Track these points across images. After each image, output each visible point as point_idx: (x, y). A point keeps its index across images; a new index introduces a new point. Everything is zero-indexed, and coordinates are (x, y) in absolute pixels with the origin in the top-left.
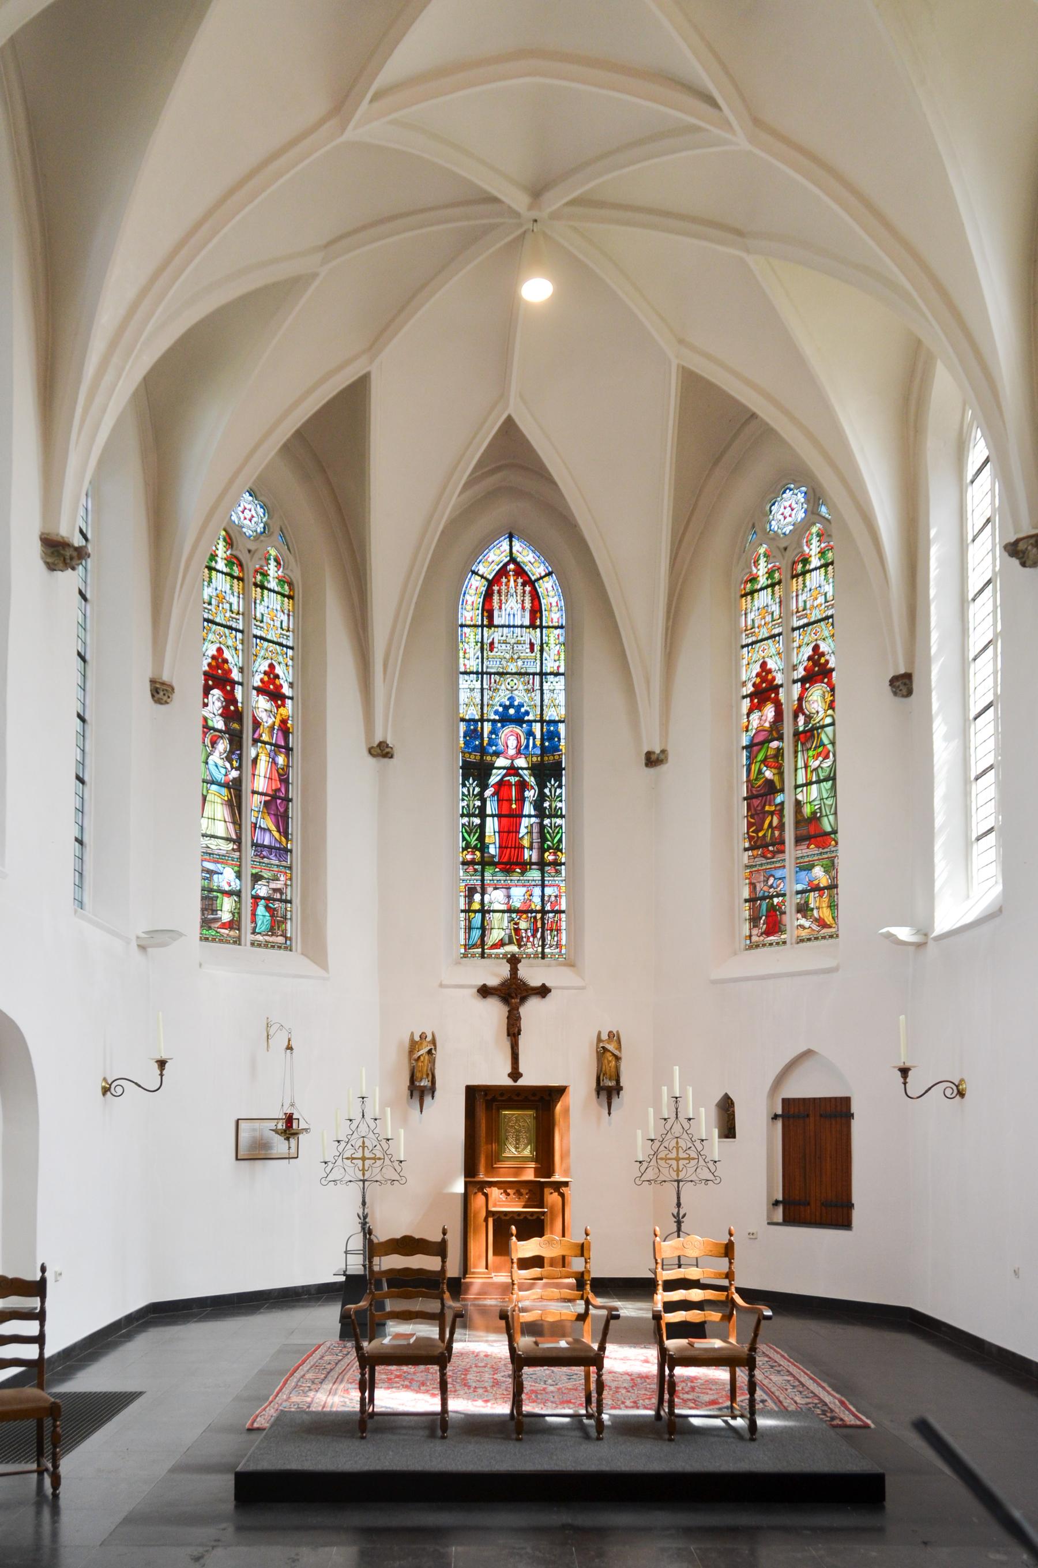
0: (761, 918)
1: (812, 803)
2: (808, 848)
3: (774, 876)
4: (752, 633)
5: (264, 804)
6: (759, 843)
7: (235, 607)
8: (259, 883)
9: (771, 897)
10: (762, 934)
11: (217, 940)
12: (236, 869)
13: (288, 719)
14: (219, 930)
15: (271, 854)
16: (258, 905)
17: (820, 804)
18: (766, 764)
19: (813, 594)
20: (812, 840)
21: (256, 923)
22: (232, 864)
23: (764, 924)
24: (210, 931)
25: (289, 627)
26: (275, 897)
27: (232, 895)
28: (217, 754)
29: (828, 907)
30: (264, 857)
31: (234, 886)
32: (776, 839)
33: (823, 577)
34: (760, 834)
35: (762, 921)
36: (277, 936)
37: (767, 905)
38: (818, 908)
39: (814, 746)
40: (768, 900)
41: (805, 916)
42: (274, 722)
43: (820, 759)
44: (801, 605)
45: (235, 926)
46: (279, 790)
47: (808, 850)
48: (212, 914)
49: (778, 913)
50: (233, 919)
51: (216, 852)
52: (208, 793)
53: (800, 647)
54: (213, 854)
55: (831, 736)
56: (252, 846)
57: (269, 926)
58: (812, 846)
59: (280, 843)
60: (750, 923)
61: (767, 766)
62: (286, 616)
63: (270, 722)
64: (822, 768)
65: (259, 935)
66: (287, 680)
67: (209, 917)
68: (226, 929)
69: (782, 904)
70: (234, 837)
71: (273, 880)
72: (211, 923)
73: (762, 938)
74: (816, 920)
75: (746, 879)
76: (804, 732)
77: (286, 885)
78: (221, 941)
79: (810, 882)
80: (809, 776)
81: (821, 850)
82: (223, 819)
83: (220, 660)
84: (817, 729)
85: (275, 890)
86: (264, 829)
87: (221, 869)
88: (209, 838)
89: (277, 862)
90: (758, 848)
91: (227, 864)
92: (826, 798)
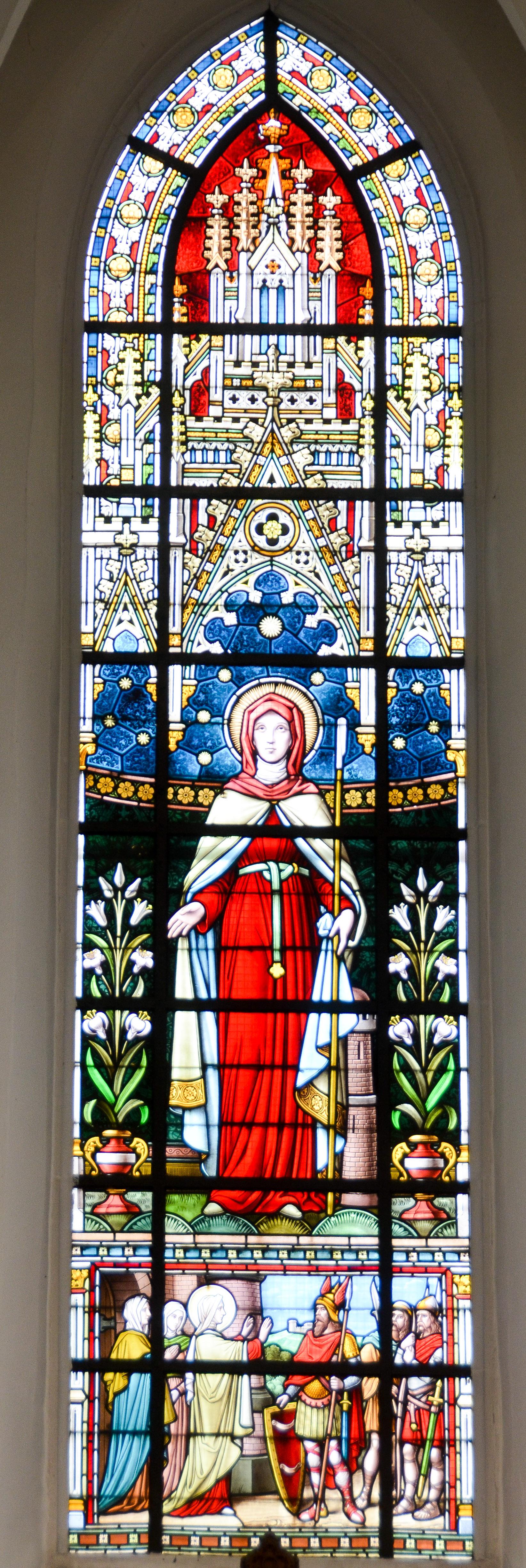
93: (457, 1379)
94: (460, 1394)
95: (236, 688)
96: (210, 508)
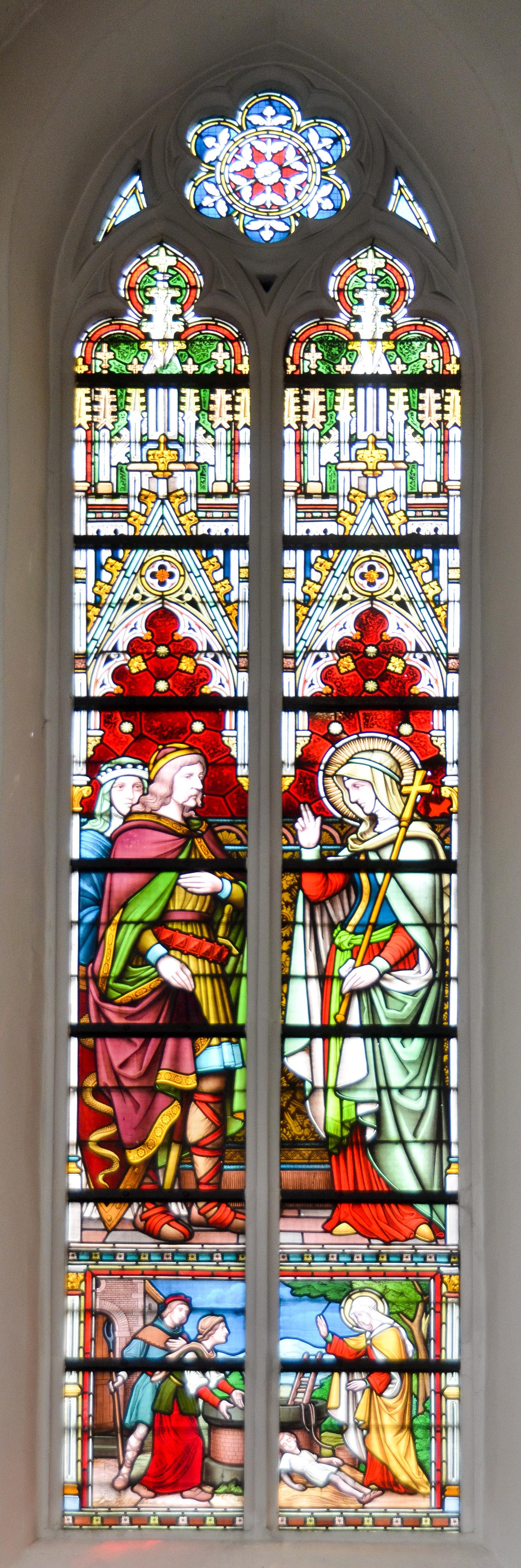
0: (129, 1431)
1: (347, 1095)
2: (328, 1229)
3: (187, 1301)
4: (113, 508)
6: (128, 1183)
9: (178, 1367)
10: (131, 1484)
17: (380, 1102)
18: (167, 934)
19: (364, 455)
20: (345, 1209)
23: (141, 1451)
25: (234, 480)
29: (402, 1427)
32: (198, 1182)
33: (400, 415)
34: (135, 1157)
35: (133, 1442)
37: (158, 1391)
38: (365, 1428)
39: (355, 920)
40: (159, 1376)
41: (310, 1445)
43: (381, 963)
44: (104, 473)
47: (326, 1238)
49: (202, 1423)
53: (307, 602)
55: (424, 903)
58: (344, 1228)
60: (84, 1440)
61: (168, 945)
64: (385, 992)
69: (220, 1394)
73: (130, 1497)
74: (356, 1464)
76: (321, 866)
79: (333, 1342)
80: (334, 1008)
81: (377, 1245)
84: (372, 868)
90: (127, 1198)
92: (401, 1090)
93: (443, 1375)
94: (447, 1386)
95: (210, 761)
96: (96, 589)
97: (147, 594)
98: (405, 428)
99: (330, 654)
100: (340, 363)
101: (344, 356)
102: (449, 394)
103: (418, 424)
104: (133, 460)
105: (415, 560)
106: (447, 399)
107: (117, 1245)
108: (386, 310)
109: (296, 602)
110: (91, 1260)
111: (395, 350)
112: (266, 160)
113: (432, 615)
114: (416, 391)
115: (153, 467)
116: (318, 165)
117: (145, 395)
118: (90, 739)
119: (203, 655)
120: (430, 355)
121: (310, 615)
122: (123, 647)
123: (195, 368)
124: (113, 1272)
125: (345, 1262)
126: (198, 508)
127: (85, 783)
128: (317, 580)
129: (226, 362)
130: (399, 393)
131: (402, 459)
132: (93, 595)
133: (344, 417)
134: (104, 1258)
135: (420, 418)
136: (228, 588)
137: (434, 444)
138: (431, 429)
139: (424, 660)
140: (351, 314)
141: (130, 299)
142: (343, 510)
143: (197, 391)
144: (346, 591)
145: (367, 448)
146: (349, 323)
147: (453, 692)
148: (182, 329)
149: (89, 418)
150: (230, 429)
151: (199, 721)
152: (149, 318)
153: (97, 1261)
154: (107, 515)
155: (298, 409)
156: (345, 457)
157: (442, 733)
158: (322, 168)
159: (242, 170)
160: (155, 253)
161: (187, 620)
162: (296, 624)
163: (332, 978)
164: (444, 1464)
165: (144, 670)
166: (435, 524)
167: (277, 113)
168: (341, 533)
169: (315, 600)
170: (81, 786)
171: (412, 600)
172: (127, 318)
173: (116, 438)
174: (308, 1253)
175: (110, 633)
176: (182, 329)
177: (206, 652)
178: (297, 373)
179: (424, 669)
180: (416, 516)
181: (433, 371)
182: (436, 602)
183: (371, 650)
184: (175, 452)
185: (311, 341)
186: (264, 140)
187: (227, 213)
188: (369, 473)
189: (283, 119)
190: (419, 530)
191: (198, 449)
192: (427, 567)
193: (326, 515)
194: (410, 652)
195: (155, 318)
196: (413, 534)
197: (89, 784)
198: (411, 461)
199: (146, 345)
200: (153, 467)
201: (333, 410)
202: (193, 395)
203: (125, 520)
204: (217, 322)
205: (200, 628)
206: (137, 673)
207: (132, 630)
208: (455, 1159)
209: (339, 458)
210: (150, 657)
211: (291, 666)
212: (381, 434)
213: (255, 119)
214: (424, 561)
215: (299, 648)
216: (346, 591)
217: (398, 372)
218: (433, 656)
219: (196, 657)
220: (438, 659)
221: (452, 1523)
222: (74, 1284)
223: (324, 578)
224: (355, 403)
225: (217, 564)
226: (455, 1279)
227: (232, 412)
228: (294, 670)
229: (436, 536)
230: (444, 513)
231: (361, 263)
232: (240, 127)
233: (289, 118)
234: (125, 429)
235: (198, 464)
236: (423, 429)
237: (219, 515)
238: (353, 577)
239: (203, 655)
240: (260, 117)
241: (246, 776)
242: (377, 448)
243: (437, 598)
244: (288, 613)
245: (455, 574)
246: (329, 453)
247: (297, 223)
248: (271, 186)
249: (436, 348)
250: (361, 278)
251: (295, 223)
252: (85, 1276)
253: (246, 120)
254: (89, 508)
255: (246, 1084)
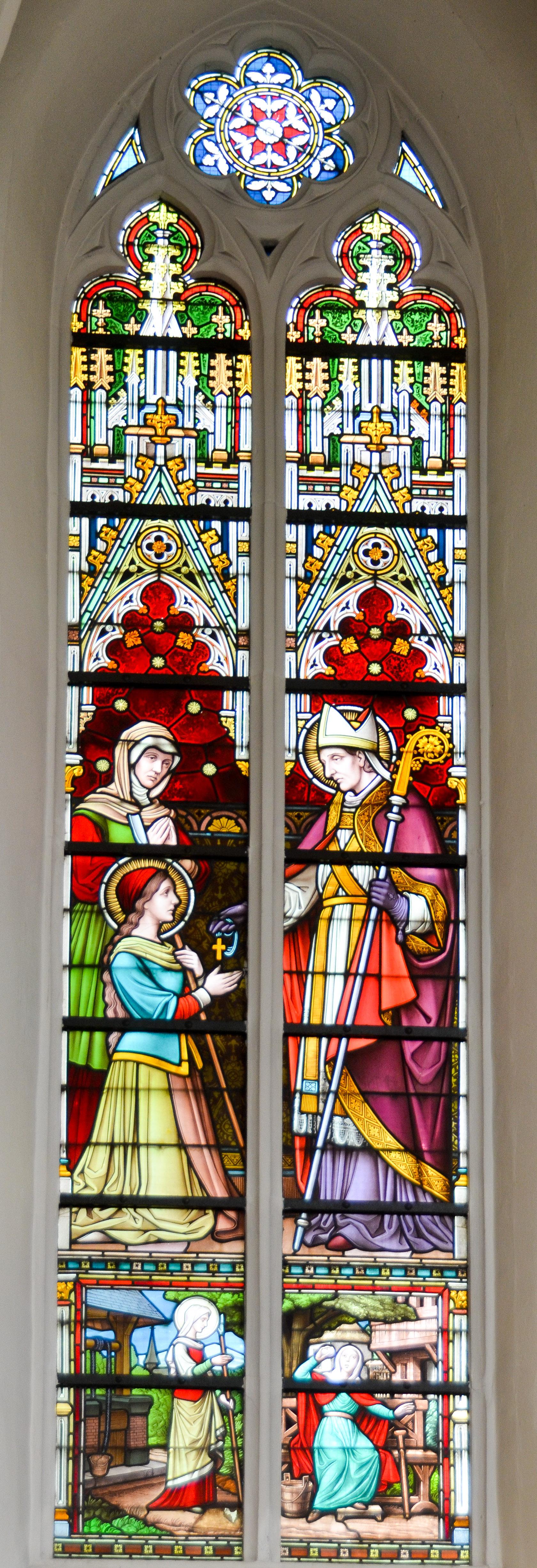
5: (345, 1063)
7: (220, 442)
8: (328, 1335)
11: (148, 1549)
12: (227, 1299)
13: (449, 762)
14: (154, 1515)
15: (380, 1230)
16: (321, 1415)
21: (313, 1478)
22: (210, 1285)
24: (117, 1522)
25: (236, 448)
26: (397, 1378)
27: (213, 1389)
28: (146, 928)
30: (349, 1245)
31: (219, 1360)
36: (409, 1516)
42: (391, 784)
45: (221, 1497)
46: (413, 1006)
48: (127, 1464)
50: (215, 1471)
51: (141, 1252)
52: (110, 1059)
53: (308, 579)
54: (129, 1261)
56: (291, 1211)
57: (370, 1484)
59: (418, 1187)
62: (436, 423)
63: (368, 782)
65: (329, 1519)
66: (440, 635)
67: (114, 1472)
68: (188, 1509)
70: (218, 1191)
71: (386, 1321)
72: (121, 1493)
75: (62, 1302)
77: (444, 1331)
78: (161, 1552)
82: (173, 1140)
83: (159, 625)
85: (394, 1356)
86: (349, 1151)
87: (166, 1308)
88: (110, 1211)
89: (405, 1257)
91: (187, 1286)
94: (455, 1410)
97: (143, 566)
98: (196, 394)
99: (117, 628)
100: (128, 322)
101: (133, 315)
102: (241, 361)
103: (424, 398)
104: (130, 424)
105: (204, 531)
106: (239, 365)
107: (200, 1255)
108: (392, 279)
109: (81, 572)
110: (80, 1268)
111: (401, 320)
112: (267, 117)
113: (438, 597)
114: (207, 356)
115: (151, 432)
116: (320, 125)
117: (144, 356)
118: (82, 715)
119: (417, 638)
120: (437, 327)
121: (96, 585)
122: (334, 627)
123: (194, 330)
124: (100, 1282)
125: (424, 1277)
126: (412, 484)
127: (78, 762)
128: (103, 550)
129: (442, 334)
130: (190, 357)
131: (192, 426)
132: (303, 571)
133: (348, 387)
134: (94, 1266)
135: (425, 392)
136: (227, 562)
137: (224, 410)
138: (222, 396)
139: (430, 643)
140: (140, 270)
141: (343, 266)
142: (346, 484)
143: (411, 362)
144: (132, 562)
145: (371, 421)
146: (139, 280)
147: (459, 678)
148: (181, 290)
149: (300, 385)
150: (445, 403)
151: (197, 701)
152: (148, 276)
153: (87, 1270)
154: (432, 492)
155: (300, 375)
156: (348, 430)
157: (232, 714)
158: (324, 129)
159: (242, 127)
160: (156, 209)
161: (400, 600)
162: (81, 596)
163: (307, 973)
164: (452, 1493)
165: (356, 651)
166: (225, 496)
167: (277, 72)
168: (343, 509)
169: (101, 570)
170: (72, 765)
171: (417, 579)
172: (342, 286)
173: (328, 407)
174: (214, 1262)
175: (321, 612)
176: (181, 290)
177: (420, 635)
178: (301, 341)
179: (213, 645)
180: (205, 487)
181: (224, 336)
182: (441, 583)
183: (375, 632)
184: (389, 425)
185: (99, 298)
186: (264, 97)
187: (229, 171)
188: (373, 447)
189: (283, 78)
190: (208, 501)
191: (197, 416)
192: (216, 539)
193: (424, 492)
194: (415, 635)
195: (154, 277)
196: (202, 505)
197: (82, 763)
198: (416, 437)
199: (360, 314)
200: (151, 432)
201: (121, 370)
202: (406, 366)
203: (122, 486)
204: (432, 291)
205: (196, 602)
206: (348, 654)
207: (343, 609)
208: (464, 1170)
209: (342, 430)
210: (363, 638)
211: (293, 645)
212: (386, 406)
213: (254, 76)
214: (213, 532)
215: (85, 620)
216: (132, 562)
217: (189, 336)
218: (222, 632)
219: (410, 640)
220: (227, 636)
221: (462, 1556)
222: (63, 1295)
223: (110, 548)
224: (144, 365)
225: (431, 545)
226: (462, 1295)
227: (447, 386)
228: (296, 649)
229: (441, 516)
230: (449, 493)
231: (366, 228)
232: (238, 83)
233: (289, 77)
234: (337, 398)
235: (198, 431)
236: (214, 396)
237: (105, 480)
238: (357, 553)
239: (417, 638)
240: (259, 74)
241: (246, 761)
242: (381, 421)
243: (442, 579)
244: (290, 591)
245: (461, 554)
246: (116, 414)
247: (300, 184)
248: (272, 145)
249: (443, 319)
250: (366, 243)
251: (297, 185)
252: (75, 1285)
253: (245, 76)
254: (301, 480)
255: (468, 1090)
